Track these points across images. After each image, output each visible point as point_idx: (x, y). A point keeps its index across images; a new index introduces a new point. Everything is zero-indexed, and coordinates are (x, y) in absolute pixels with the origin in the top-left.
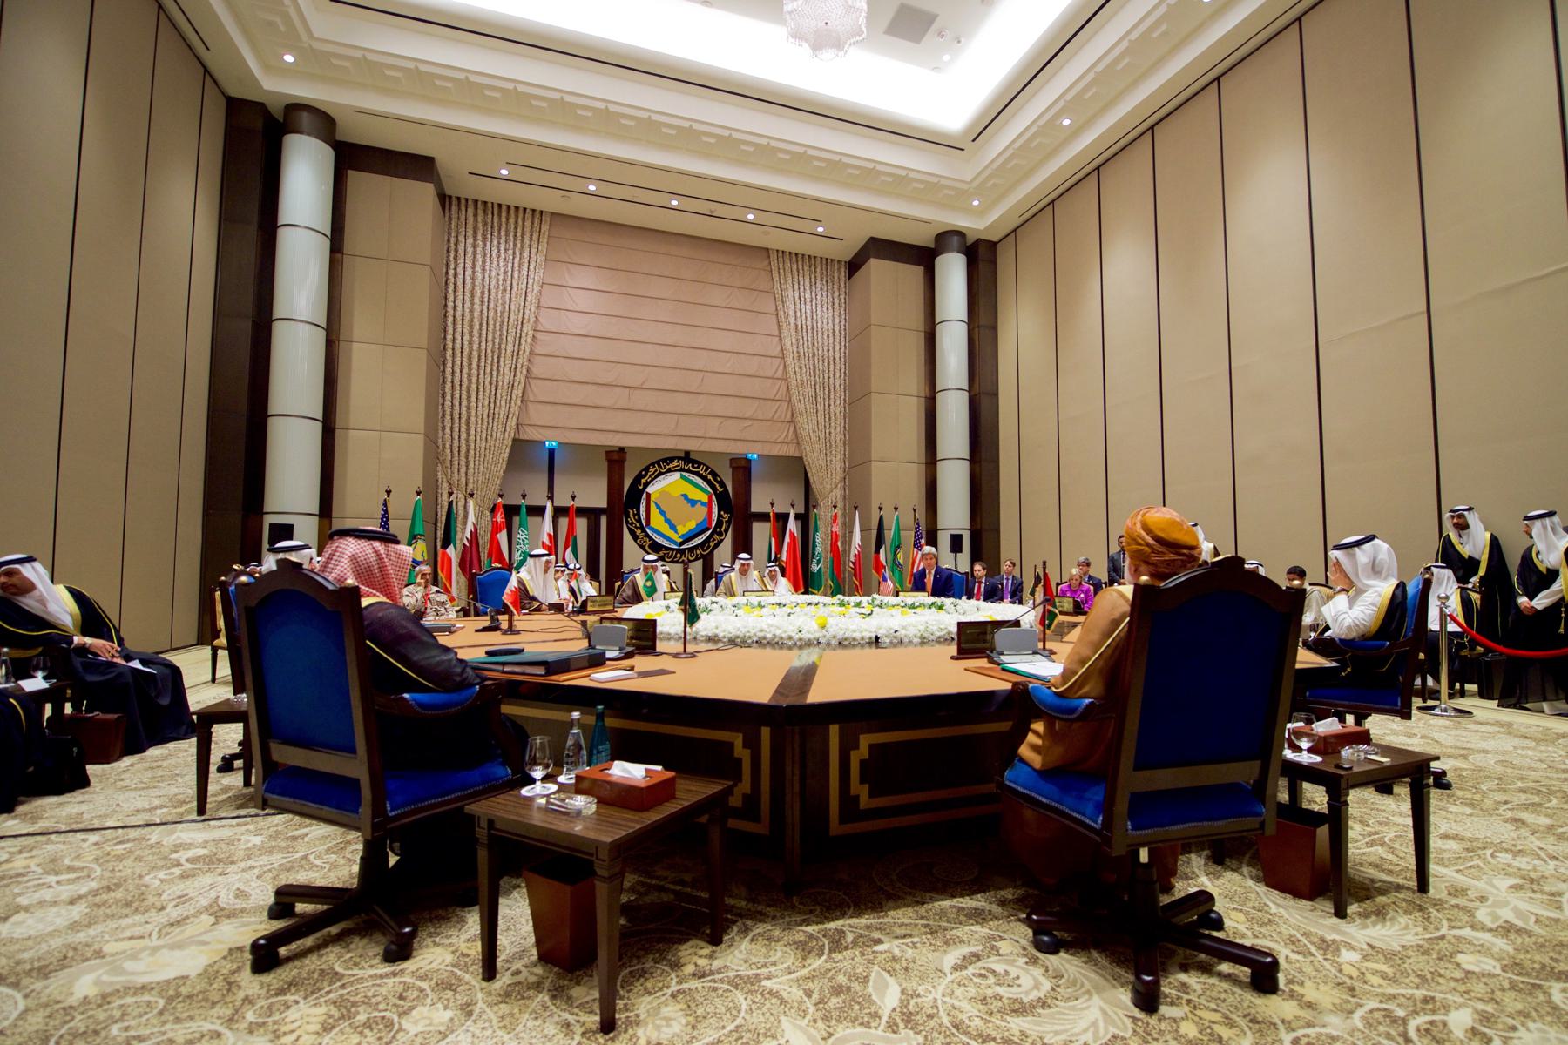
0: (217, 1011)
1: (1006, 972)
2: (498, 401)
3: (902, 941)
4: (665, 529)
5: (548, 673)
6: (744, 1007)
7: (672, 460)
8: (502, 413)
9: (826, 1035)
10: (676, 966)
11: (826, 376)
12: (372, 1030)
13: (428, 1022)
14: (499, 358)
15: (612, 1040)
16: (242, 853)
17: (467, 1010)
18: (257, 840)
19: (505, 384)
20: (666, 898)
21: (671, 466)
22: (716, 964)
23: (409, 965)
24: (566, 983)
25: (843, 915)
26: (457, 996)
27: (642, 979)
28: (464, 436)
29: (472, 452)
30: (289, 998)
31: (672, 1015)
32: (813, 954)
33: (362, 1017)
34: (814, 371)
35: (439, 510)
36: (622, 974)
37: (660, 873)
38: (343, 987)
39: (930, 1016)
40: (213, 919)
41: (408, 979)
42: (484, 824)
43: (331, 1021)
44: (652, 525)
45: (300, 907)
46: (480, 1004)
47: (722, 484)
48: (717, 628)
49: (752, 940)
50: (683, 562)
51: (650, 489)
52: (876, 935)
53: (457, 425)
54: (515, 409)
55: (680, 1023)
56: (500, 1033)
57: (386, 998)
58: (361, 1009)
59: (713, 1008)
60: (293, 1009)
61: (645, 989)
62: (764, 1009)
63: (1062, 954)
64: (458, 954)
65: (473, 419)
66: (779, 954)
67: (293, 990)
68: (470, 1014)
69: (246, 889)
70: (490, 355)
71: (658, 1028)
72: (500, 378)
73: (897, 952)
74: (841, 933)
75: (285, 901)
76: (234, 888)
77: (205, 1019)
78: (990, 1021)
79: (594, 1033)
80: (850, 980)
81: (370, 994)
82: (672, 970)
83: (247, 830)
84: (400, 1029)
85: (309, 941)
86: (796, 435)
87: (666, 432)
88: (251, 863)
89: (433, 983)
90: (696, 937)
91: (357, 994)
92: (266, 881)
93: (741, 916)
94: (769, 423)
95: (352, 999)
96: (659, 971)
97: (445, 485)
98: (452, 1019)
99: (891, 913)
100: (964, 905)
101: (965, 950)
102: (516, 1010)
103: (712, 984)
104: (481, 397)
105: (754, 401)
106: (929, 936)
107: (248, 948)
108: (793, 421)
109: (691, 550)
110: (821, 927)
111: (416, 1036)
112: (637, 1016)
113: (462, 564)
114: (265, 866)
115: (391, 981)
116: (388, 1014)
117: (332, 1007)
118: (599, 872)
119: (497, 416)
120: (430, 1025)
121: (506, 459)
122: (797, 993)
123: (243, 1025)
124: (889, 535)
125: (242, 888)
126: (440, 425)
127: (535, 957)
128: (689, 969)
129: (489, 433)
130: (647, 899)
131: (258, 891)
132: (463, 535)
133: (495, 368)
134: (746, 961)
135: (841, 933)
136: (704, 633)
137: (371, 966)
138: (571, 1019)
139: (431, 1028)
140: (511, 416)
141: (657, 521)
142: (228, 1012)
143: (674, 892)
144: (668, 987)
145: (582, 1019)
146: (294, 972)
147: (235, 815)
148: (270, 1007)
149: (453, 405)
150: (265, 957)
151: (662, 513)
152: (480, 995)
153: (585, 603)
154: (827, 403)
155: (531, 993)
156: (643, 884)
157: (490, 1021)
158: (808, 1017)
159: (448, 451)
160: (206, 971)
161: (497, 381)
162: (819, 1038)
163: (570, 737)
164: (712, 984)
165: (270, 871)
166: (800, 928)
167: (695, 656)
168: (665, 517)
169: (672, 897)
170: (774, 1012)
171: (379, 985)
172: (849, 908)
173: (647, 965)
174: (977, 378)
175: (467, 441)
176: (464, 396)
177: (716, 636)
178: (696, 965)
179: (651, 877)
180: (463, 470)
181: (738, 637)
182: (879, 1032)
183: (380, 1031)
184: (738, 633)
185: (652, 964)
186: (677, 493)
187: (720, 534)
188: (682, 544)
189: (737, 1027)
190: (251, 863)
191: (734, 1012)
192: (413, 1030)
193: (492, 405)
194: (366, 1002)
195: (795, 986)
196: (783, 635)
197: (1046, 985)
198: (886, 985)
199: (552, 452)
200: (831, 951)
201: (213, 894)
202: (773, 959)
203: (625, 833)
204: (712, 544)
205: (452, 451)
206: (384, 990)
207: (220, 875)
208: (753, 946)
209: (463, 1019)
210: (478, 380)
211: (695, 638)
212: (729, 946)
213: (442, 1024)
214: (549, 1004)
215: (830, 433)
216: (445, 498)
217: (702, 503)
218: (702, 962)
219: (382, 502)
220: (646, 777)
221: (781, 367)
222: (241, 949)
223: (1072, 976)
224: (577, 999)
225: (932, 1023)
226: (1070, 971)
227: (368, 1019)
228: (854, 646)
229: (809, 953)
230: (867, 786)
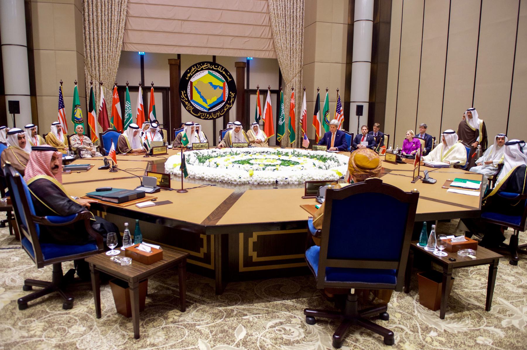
0: (9, 321)
1: (290, 330)
2: (112, 31)
3: (254, 316)
4: (200, 101)
5: (119, 203)
6: (187, 334)
7: (203, 63)
8: (115, 37)
9: (212, 346)
10: (166, 318)
11: (292, 11)
12: (59, 331)
13: (77, 330)
14: (111, 6)
15: (138, 341)
16: (12, 264)
17: (91, 328)
18: (17, 259)
19: (116, 20)
20: (169, 292)
21: (203, 67)
22: (181, 319)
23: (72, 311)
24: (126, 321)
25: (236, 304)
26: (88, 323)
27: (153, 322)
28: (96, 51)
29: (101, 59)
30: (32, 319)
31: (161, 335)
32: (219, 318)
33: (56, 327)
34: (285, 8)
35: (87, 90)
36: (146, 320)
37: (169, 282)
38: (49, 317)
39: (253, 343)
40: (4, 290)
41: (71, 316)
42: (92, 265)
43: (46, 328)
44: (194, 99)
45: (34, 287)
46: (95, 326)
47: (231, 76)
48: (204, 173)
49: (197, 311)
50: (212, 119)
51: (192, 80)
52: (245, 313)
53: (92, 44)
54: (121, 35)
55: (162, 338)
56: (101, 336)
57: (64, 322)
58: (56, 324)
59: (175, 334)
60: (33, 323)
61: (153, 326)
62: (194, 336)
63: (316, 325)
64: (89, 308)
65: (100, 41)
66: (206, 317)
67: (33, 317)
68: (91, 329)
69: (15, 279)
70: (107, 4)
71: (155, 339)
72: (113, 17)
73: (251, 319)
74: (232, 311)
75: (28, 285)
76: (11, 278)
77: (6, 324)
78: (274, 346)
79: (132, 339)
80: (229, 328)
81: (58, 320)
82: (164, 319)
83: (13, 254)
84: (68, 332)
85: (38, 300)
86: (274, 48)
87: (202, 45)
88: (15, 268)
89: (80, 317)
90: (176, 308)
91: (54, 319)
92: (22, 276)
93: (196, 301)
94: (259, 39)
95: (53, 321)
96: (159, 320)
97: (89, 77)
98: (85, 330)
99: (255, 304)
100: (286, 303)
101: (277, 321)
102: (107, 329)
103: (178, 326)
104: (103, 28)
105: (250, 26)
106: (266, 314)
107: (17, 301)
108: (272, 38)
109: (215, 112)
110: (225, 308)
111: (73, 334)
112: (148, 334)
113: (99, 120)
114: (21, 270)
115: (65, 316)
116: (64, 327)
117: (46, 323)
118: (131, 287)
119: (112, 39)
120: (78, 331)
121: (118, 62)
122: (208, 331)
123: (18, 327)
124: (323, 104)
125: (13, 278)
126: (84, 44)
127: (116, 311)
128: (171, 320)
129: (109, 48)
130: (161, 293)
131: (19, 279)
132: (99, 104)
133: (110, 12)
134: (192, 319)
135: (232, 311)
136: (198, 176)
137: (59, 310)
138: (125, 333)
139: (78, 333)
140: (119, 38)
141: (196, 97)
142: (13, 322)
143: (173, 291)
144: (161, 325)
145: (129, 334)
146: (33, 310)
147: (8, 247)
148: (26, 322)
149: (90, 33)
150: (23, 304)
151: (199, 93)
152: (95, 323)
153: (152, 151)
154: (292, 27)
155: (113, 324)
156: (161, 286)
157: (98, 332)
158: (209, 340)
159: (89, 59)
160: (4, 308)
161: (111, 19)
162: (210, 346)
163: (125, 232)
164: (178, 326)
165: (22, 272)
166: (217, 308)
167: (187, 192)
168: (200, 95)
169: (171, 292)
170: (197, 337)
171: (61, 317)
172: (239, 301)
173: (156, 317)
174: (378, 15)
175: (98, 53)
176: (95, 28)
177: (203, 177)
178: (174, 319)
179: (165, 284)
180: (97, 69)
181: (213, 179)
182: (232, 347)
183: (62, 332)
184: (213, 177)
185: (157, 317)
186: (206, 82)
187: (230, 104)
188: (210, 109)
189: (182, 341)
190: (15, 268)
191: (183, 336)
192: (72, 333)
193: (110, 33)
194: (57, 322)
195: (207, 329)
196: (233, 179)
197: (303, 335)
198: (242, 331)
199: (142, 57)
200: (225, 318)
201: (3, 280)
202: (202, 319)
203: (139, 274)
204: (225, 109)
205: (91, 59)
206: (63, 319)
207: (5, 272)
208: (197, 313)
209: (89, 330)
210: (102, 19)
211: (194, 178)
212: (188, 313)
213: (82, 331)
214: (119, 328)
215: (293, 45)
216: (89, 86)
217: (220, 87)
218: (176, 318)
219: (59, 88)
220: (151, 251)
221: (266, 6)
222: (14, 301)
223: (315, 333)
224: (129, 327)
225: (253, 345)
226: (315, 331)
227: (58, 328)
228: (265, 185)
229: (217, 317)
230: (256, 253)
